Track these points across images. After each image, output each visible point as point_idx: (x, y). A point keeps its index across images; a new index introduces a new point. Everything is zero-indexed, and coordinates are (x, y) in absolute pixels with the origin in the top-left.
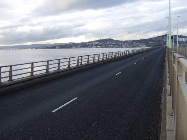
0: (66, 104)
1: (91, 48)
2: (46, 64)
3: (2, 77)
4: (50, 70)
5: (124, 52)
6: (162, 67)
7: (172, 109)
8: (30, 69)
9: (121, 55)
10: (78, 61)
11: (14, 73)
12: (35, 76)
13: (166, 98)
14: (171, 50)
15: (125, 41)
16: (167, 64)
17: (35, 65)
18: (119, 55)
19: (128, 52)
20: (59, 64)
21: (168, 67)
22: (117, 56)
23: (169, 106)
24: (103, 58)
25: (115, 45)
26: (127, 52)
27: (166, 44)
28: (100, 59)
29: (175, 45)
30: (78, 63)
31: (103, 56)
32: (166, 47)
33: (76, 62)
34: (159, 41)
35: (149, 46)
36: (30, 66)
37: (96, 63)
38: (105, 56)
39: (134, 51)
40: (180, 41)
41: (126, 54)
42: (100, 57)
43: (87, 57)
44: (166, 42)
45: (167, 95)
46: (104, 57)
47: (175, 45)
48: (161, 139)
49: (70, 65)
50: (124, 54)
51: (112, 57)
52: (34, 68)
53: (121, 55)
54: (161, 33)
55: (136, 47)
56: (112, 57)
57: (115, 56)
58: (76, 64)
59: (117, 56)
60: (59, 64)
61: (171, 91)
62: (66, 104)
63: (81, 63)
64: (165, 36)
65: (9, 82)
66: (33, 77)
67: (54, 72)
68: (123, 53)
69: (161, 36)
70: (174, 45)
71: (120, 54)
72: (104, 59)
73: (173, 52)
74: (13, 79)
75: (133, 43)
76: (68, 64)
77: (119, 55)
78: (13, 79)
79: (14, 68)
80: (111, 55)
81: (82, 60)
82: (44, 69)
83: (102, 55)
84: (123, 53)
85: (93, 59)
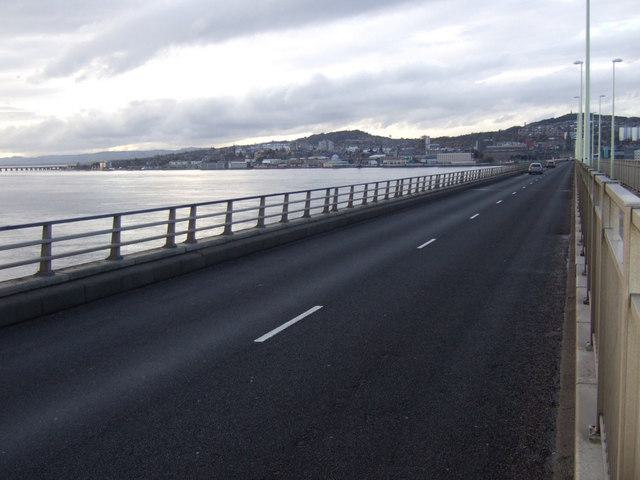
0: (294, 321)
1: (227, 168)
2: (111, 227)
3: (53, 254)
4: (198, 235)
5: (428, 178)
6: (563, 227)
7: (600, 413)
8: (109, 236)
9: (417, 191)
10: (327, 200)
11: (56, 249)
12: (199, 242)
13: (573, 260)
14: (593, 173)
15: (461, 137)
16: (577, 226)
17: (125, 222)
18: (413, 191)
19: (441, 181)
20: (286, 206)
21: (580, 226)
22: (405, 193)
23: (585, 394)
24: (365, 200)
25: (329, 155)
26: (438, 181)
27: (570, 148)
28: (354, 203)
29: (606, 156)
30: (326, 208)
31: (388, 190)
32: (574, 165)
34: (543, 138)
35: (490, 161)
36: (108, 224)
37: (269, 232)
38: (371, 194)
40: (634, 139)
41: (437, 186)
42: (355, 196)
43: (304, 196)
44: (571, 143)
45: (577, 439)
46: (380, 192)
47: (606, 156)
49: (230, 226)
50: (417, 190)
52: (122, 233)
53: (420, 190)
54: (558, 111)
55: (425, 165)
56: (409, 191)
57: (396, 194)
58: (163, 242)
59: (405, 193)
62: (294, 321)
63: (335, 206)
64: (572, 117)
65: (109, 262)
66: (229, 237)
67: (78, 273)
68: (418, 185)
69: (552, 121)
70: (617, 157)
71: (414, 186)
74: (122, 254)
75: (415, 152)
76: (323, 204)
77: (413, 191)
78: (122, 254)
79: (57, 230)
81: (336, 198)
82: (300, 208)
83: (348, 190)
84: (418, 185)
85: (280, 209)
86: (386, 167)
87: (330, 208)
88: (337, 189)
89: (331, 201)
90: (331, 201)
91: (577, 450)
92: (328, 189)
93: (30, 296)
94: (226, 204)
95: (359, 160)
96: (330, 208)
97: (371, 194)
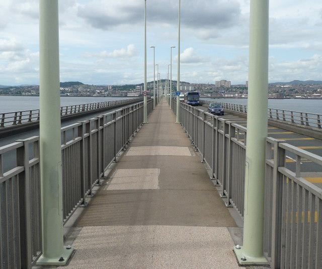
10: (15, 118)
15: (70, 82)
20: (30, 116)
26: (98, 105)
30: (15, 122)
33: (13, 119)
39: (98, 105)
46: (68, 110)
48: (249, 2)
51: (66, 113)
56: (66, 113)
60: (30, 116)
61: (214, 172)
63: (20, 121)
71: (89, 107)
72: (68, 113)
73: (110, 54)
80: (70, 110)
81: (20, 117)
85: (28, 117)
86: (82, 96)
87: (17, 122)
88: (21, 112)
89: (18, 118)
90: (18, 118)
91: (116, 227)
92: (16, 113)
93: (6, 131)
94: (29, 112)
95: (77, 94)
96: (17, 122)
97: (73, 110)
